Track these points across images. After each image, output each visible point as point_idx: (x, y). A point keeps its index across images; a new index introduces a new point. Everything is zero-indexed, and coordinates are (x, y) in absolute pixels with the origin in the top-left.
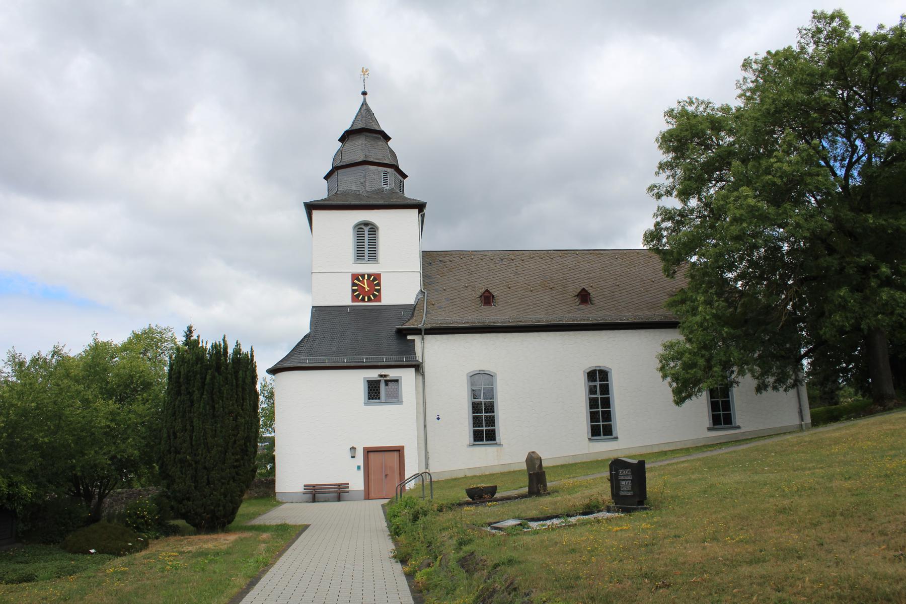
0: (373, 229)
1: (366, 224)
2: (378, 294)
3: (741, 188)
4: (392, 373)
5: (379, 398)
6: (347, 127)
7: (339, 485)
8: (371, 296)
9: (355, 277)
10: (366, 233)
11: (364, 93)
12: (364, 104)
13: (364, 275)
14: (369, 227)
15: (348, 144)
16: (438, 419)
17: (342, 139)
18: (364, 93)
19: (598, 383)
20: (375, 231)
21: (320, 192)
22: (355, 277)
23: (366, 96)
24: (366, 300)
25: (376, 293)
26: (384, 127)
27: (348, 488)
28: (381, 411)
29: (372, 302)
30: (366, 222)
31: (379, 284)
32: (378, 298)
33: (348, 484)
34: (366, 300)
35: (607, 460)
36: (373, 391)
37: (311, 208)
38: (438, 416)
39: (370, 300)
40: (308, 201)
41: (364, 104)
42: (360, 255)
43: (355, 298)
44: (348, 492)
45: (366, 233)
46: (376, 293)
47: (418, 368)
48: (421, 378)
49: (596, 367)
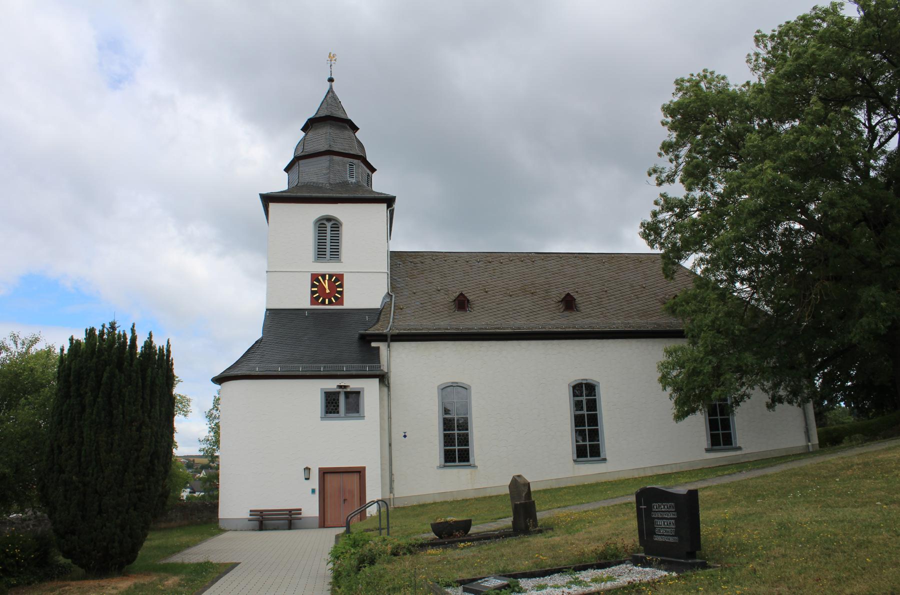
0: (336, 225)
1: (329, 219)
4: (353, 384)
5: (338, 412)
6: (312, 114)
7: (290, 511)
9: (315, 277)
10: (329, 229)
11: (331, 80)
12: (331, 91)
13: (312, 291)
16: (405, 436)
17: (304, 129)
18: (331, 80)
19: (584, 398)
20: (338, 227)
21: (280, 183)
22: (315, 277)
24: (327, 302)
27: (300, 514)
28: (341, 426)
29: (332, 305)
30: (328, 217)
31: (341, 286)
32: (340, 301)
33: (300, 510)
34: (327, 302)
36: (331, 404)
37: (268, 199)
38: (405, 433)
39: (331, 303)
40: (265, 191)
41: (331, 91)
42: (320, 254)
43: (314, 301)
44: (300, 519)
47: (383, 379)
48: (386, 389)
49: (582, 380)
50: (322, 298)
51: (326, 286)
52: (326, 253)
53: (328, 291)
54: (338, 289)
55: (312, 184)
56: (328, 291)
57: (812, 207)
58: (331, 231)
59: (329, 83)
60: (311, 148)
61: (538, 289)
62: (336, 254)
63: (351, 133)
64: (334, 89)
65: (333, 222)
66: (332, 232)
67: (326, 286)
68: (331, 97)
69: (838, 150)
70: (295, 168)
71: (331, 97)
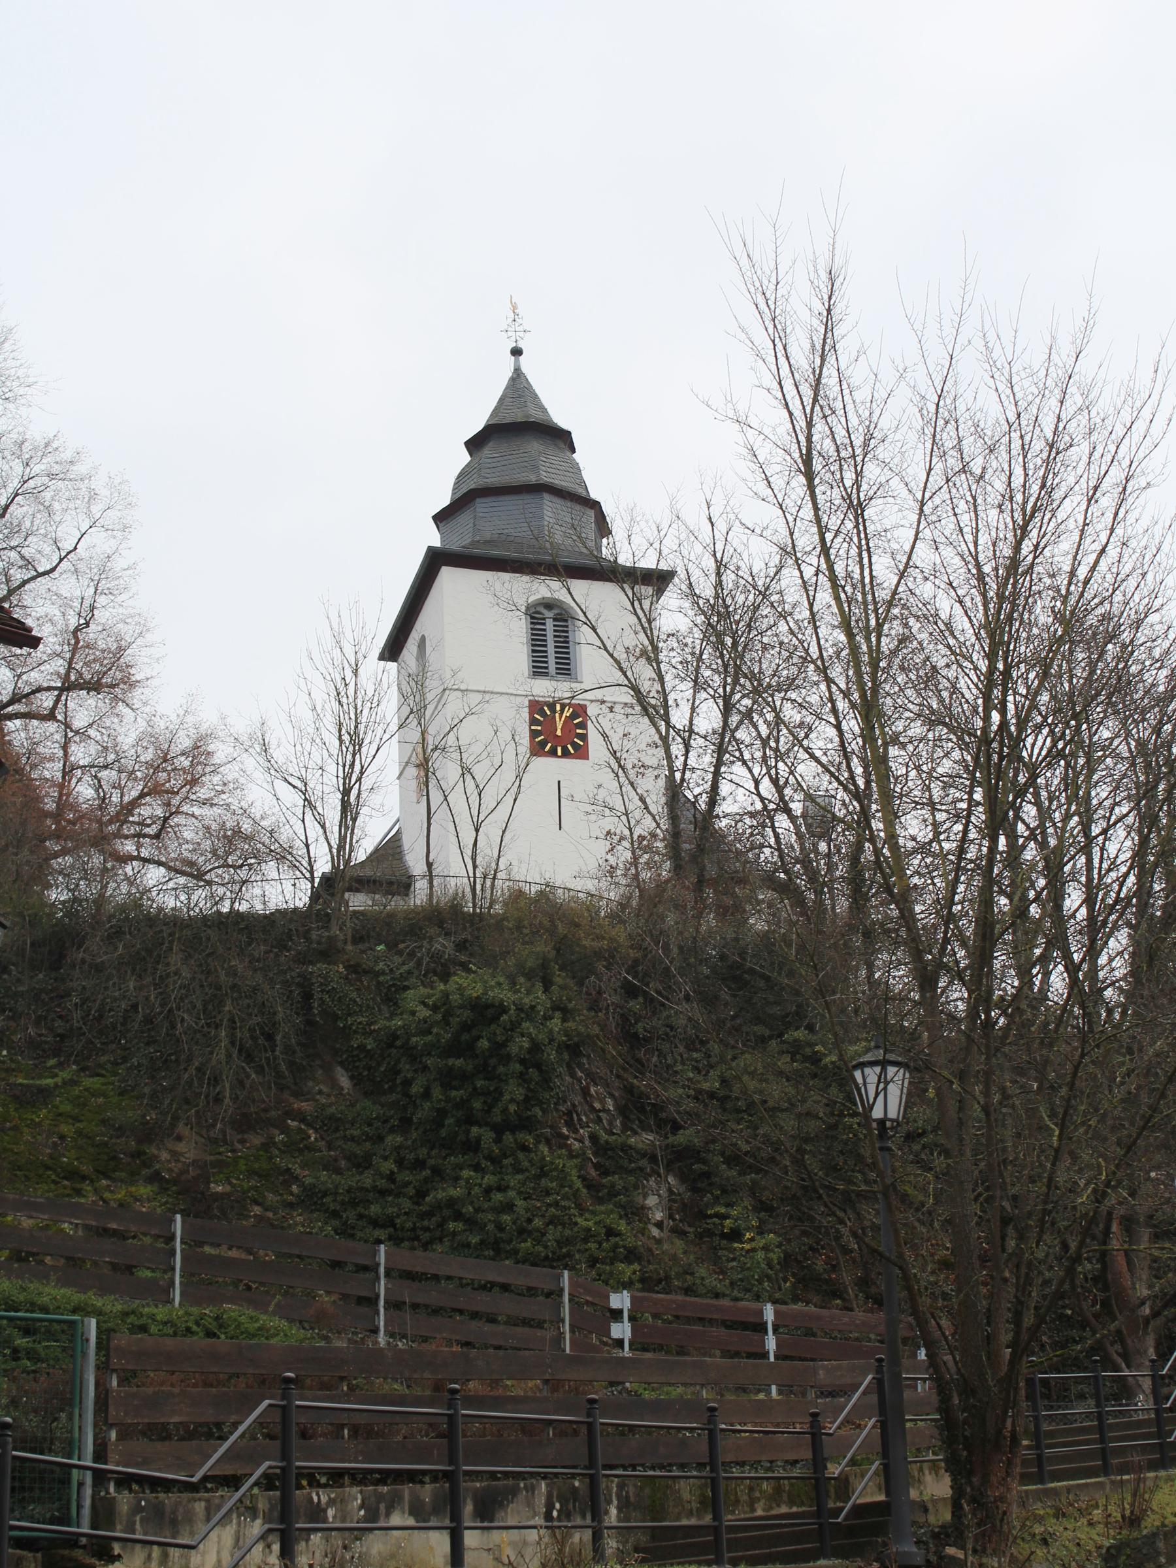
1: (549, 605)
9: (536, 707)
11: (517, 352)
12: (518, 375)
13: (531, 730)
18: (517, 352)
22: (536, 707)
31: (566, 754)
41: (518, 375)
42: (539, 669)
51: (559, 725)
52: (554, 655)
55: (512, 539)
56: (559, 733)
57: (1002, 1021)
58: (545, 646)
61: (1056, 894)
62: (566, 668)
63: (568, 454)
65: (556, 611)
67: (559, 725)
68: (518, 386)
69: (856, 977)
70: (487, 452)
71: (518, 386)
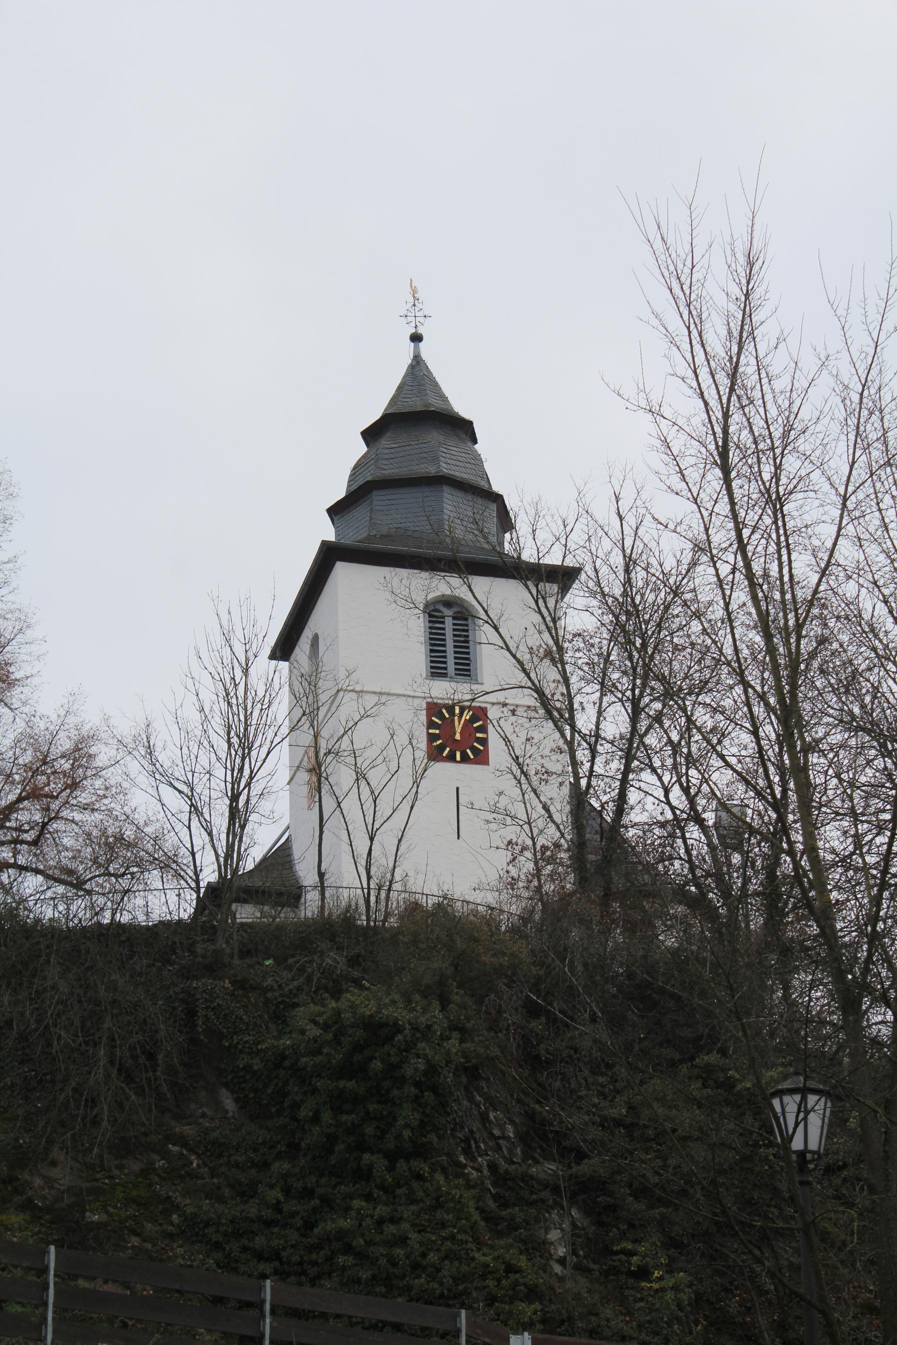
1: (448, 602)
2: (482, 748)
3: (507, 546)
6: (375, 415)
8: (468, 751)
9: (433, 709)
10: (449, 622)
11: (416, 338)
12: (417, 362)
13: (429, 734)
14: (455, 609)
15: (385, 442)
17: (371, 435)
18: (416, 338)
20: (431, 639)
22: (433, 709)
23: (421, 345)
25: (479, 746)
26: (462, 407)
31: (465, 759)
34: (458, 758)
35: (445, 399)
41: (417, 362)
42: (437, 671)
45: (449, 622)
46: (479, 746)
50: (475, 725)
53: (458, 737)
54: (478, 735)
58: (444, 646)
59: (412, 344)
60: (390, 470)
63: (470, 444)
64: (424, 356)
66: (433, 654)
